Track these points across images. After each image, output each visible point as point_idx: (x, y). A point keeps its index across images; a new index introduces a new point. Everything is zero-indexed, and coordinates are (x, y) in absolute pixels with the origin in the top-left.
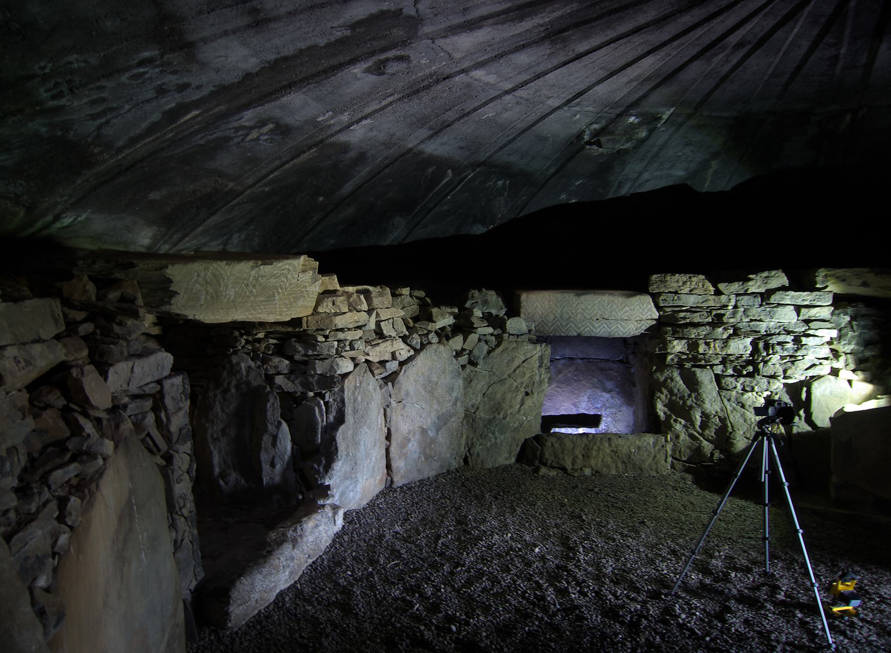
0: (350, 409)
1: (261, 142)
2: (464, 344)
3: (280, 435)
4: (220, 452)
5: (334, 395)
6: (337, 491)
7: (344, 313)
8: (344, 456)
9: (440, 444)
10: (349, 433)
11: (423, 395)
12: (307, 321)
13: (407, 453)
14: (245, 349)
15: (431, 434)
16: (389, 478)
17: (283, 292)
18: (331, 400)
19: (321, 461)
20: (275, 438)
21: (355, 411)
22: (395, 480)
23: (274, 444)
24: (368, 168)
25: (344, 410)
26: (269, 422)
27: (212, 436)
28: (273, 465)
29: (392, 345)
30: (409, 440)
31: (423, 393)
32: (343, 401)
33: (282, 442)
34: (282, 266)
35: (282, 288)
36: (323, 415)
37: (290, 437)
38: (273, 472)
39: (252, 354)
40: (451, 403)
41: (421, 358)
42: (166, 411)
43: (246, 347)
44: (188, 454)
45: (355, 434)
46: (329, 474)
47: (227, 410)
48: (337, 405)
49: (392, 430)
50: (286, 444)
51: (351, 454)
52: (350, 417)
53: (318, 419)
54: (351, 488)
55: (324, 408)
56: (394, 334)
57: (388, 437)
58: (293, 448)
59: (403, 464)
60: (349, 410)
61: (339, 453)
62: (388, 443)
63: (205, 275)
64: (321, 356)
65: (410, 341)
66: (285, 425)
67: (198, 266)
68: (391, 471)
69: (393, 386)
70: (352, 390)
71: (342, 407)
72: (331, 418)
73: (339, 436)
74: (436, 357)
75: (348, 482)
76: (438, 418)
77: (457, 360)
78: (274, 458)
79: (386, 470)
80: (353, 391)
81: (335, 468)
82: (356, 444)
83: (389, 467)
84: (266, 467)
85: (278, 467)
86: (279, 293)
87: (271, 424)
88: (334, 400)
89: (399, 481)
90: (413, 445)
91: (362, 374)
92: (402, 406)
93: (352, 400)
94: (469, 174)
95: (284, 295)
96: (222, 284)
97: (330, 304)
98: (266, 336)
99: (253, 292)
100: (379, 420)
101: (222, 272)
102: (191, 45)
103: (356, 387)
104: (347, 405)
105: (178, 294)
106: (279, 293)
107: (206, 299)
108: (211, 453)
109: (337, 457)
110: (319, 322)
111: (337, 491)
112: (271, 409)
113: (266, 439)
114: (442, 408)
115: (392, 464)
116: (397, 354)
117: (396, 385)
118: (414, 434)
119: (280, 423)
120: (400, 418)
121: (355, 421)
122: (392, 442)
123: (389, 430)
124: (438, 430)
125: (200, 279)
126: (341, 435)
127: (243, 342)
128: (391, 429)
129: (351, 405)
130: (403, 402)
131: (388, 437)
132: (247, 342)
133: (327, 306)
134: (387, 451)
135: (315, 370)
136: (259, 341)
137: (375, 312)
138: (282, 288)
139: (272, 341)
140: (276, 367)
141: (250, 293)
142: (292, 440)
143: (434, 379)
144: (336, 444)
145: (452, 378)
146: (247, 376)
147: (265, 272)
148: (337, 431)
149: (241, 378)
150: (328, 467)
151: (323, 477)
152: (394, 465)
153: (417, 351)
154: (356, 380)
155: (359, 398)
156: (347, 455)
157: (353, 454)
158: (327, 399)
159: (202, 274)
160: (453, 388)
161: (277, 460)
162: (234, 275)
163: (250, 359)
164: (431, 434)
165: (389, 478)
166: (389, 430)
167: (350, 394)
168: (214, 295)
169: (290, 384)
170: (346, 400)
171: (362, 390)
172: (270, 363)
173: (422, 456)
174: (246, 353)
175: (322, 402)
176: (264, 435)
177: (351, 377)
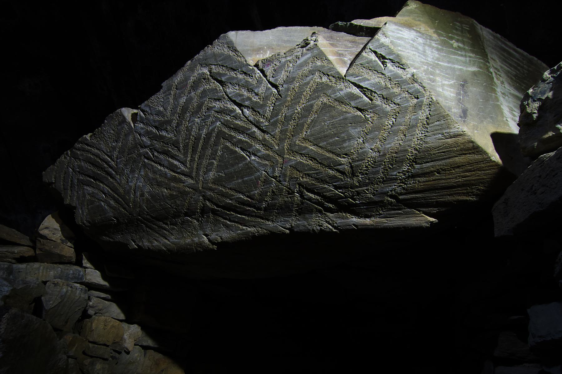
35: (238, 129)
138: (238, 129)
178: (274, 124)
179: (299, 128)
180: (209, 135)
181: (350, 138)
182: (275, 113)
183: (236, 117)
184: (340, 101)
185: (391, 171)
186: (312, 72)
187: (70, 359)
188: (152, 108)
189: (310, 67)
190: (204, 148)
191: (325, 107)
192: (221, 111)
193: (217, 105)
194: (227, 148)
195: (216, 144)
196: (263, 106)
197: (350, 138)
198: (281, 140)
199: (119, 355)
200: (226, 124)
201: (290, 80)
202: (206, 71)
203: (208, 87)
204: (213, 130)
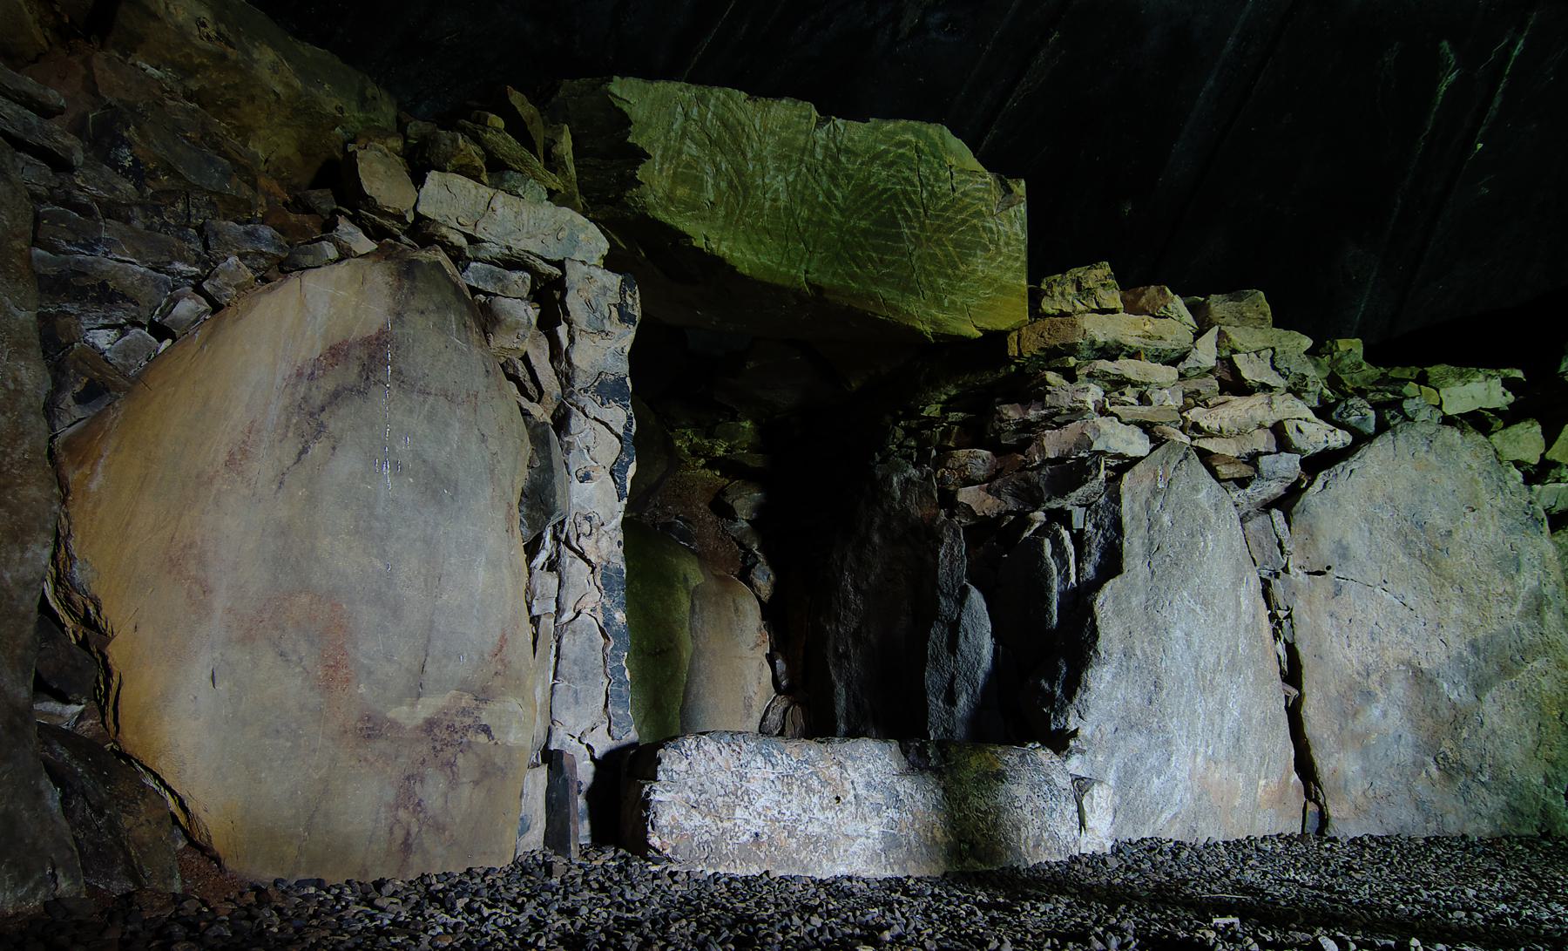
0: (1137, 542)
1: (933, 35)
2: (1548, 446)
3: (965, 620)
4: (848, 686)
5: (1096, 512)
6: (1107, 761)
7: (1114, 311)
8: (1117, 655)
9: (1494, 732)
10: (1135, 601)
11: (1402, 565)
12: (1019, 338)
13: (1367, 734)
14: (904, 450)
15: (1455, 692)
16: (1312, 807)
17: (917, 214)
18: (1089, 527)
19: (1058, 669)
20: (954, 628)
21: (1152, 549)
22: (1332, 811)
23: (953, 646)
24: (1211, 83)
25: (1121, 544)
26: (942, 592)
27: (836, 649)
28: (951, 699)
29: (1270, 404)
30: (1368, 696)
31: (1403, 559)
32: (1117, 525)
33: (970, 636)
34: (895, 133)
35: (911, 203)
36: (1067, 563)
37: (989, 625)
38: (951, 714)
39: (915, 455)
40: (1518, 608)
41: (1375, 457)
42: (570, 325)
43: (906, 443)
44: (618, 436)
45: (1151, 607)
46: (1076, 701)
47: (864, 586)
48: (1103, 535)
49: (1304, 651)
50: (981, 643)
51: (1138, 653)
52: (1138, 562)
53: (1048, 565)
54: (1152, 760)
55: (1071, 549)
56: (1273, 379)
57: (1292, 673)
58: (996, 651)
59: (1356, 768)
60: (1133, 545)
61: (1102, 644)
62: (1295, 692)
63: (702, 118)
64: (1056, 419)
65: (1340, 415)
66: (976, 598)
67: (681, 90)
68: (1317, 784)
69: (1288, 522)
70: (1143, 498)
71: (1117, 537)
72: (1089, 569)
73: (1105, 602)
74: (1432, 458)
75: (1142, 739)
76: (1474, 647)
77: (1531, 490)
78: (953, 678)
79: (1295, 777)
80: (1147, 501)
81: (1092, 684)
82: (1158, 631)
83: (1305, 766)
84: (936, 704)
85: (963, 701)
86: (907, 218)
87: (947, 596)
88: (1096, 526)
89: (1347, 823)
90: (1385, 714)
91: (1174, 463)
92: (1332, 589)
93: (1145, 523)
94: (1513, 44)
95: (923, 227)
96: (750, 155)
97: (1071, 290)
98: (944, 411)
99: (835, 197)
100: (1244, 602)
101: (742, 116)
102: (1367, 729)
103: (1155, 492)
104: (1127, 532)
105: (649, 157)
106: (907, 218)
107: (716, 186)
108: (833, 686)
109: (1096, 651)
110: (1046, 334)
111: (1107, 761)
112: (946, 562)
113: (937, 633)
114: (1483, 618)
115: (1318, 762)
116: (1290, 429)
117: (1296, 518)
118: (1385, 681)
119: (965, 592)
120: (1326, 624)
121: (1153, 573)
122: (1305, 688)
123: (1291, 649)
124: (1479, 688)
125: (693, 128)
126: (1110, 600)
127: (900, 433)
128: (1298, 647)
129: (1143, 532)
130: (1332, 574)
131: (1292, 673)
132: (909, 432)
133: (1062, 294)
134: (1294, 713)
135: (1042, 449)
136: (930, 422)
137: (1216, 328)
138: (911, 203)
139: (954, 416)
140: (963, 467)
141: (828, 198)
142: (995, 634)
143: (1438, 519)
144: (1094, 620)
145: (1510, 531)
146: (903, 499)
147: (851, 139)
148: (1098, 591)
149: (892, 508)
150: (1074, 684)
151: (1061, 710)
152: (1325, 764)
153: (1361, 439)
154: (1155, 476)
155: (1166, 519)
156: (1128, 654)
157: (1144, 653)
158: (1077, 523)
159: (695, 113)
160: (1516, 558)
161: (960, 683)
162: (773, 133)
163: (911, 466)
164: (1455, 692)
165: (1312, 807)
166: (1291, 649)
167: (1137, 508)
168: (736, 181)
169: (990, 500)
170: (1126, 519)
171: (1173, 498)
172: (950, 464)
173: (1430, 760)
174: (904, 457)
175: (1065, 534)
176: (932, 625)
177: (1138, 468)
178: (938, 217)
179: (951, 230)
180: (885, 191)
181: (975, 255)
182: (945, 209)
183: (915, 192)
184: (984, 228)
185: (1392, 901)
186: (981, 199)
187: (185, 903)
188: (941, 281)
189: (981, 194)
190: (872, 198)
191: (974, 228)
192: (907, 180)
193: (907, 173)
194: (891, 209)
195: (886, 201)
196: (939, 198)
197: (975, 255)
198: (935, 231)
199: (597, 260)
200: (904, 192)
201: (965, 194)
202: (914, 140)
203: (908, 153)
204: (890, 189)
